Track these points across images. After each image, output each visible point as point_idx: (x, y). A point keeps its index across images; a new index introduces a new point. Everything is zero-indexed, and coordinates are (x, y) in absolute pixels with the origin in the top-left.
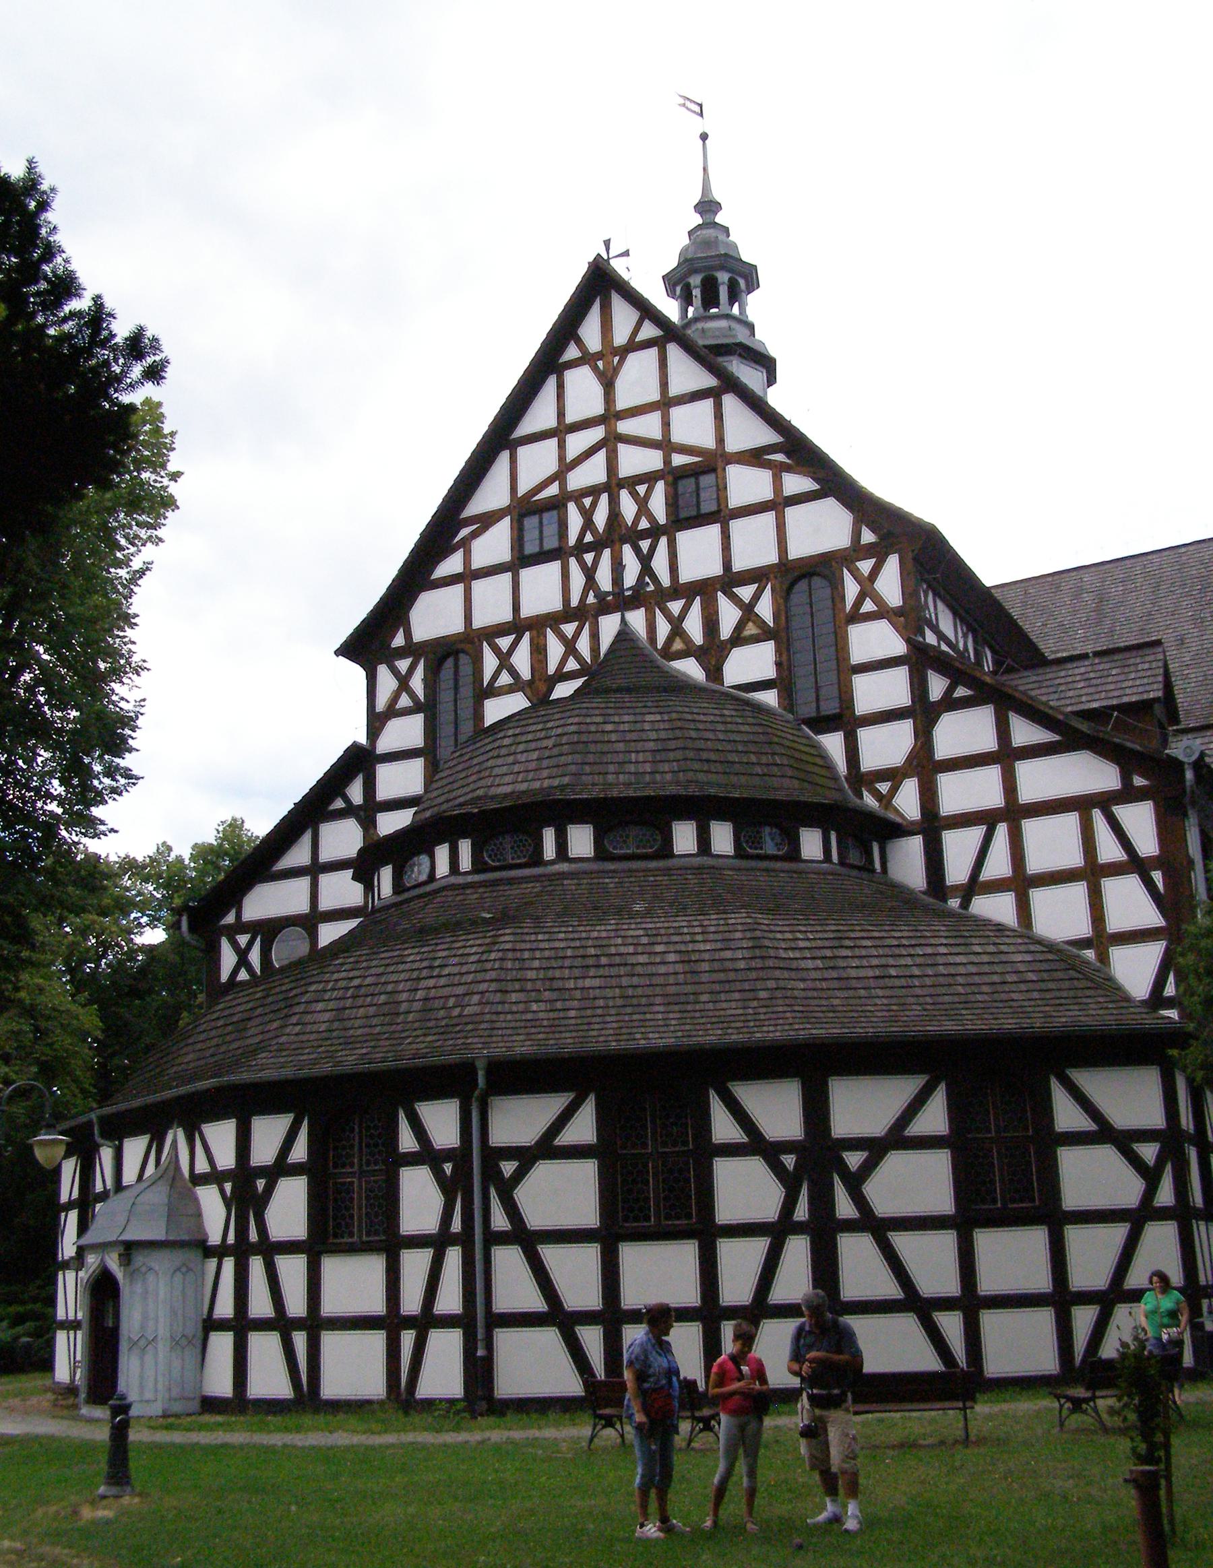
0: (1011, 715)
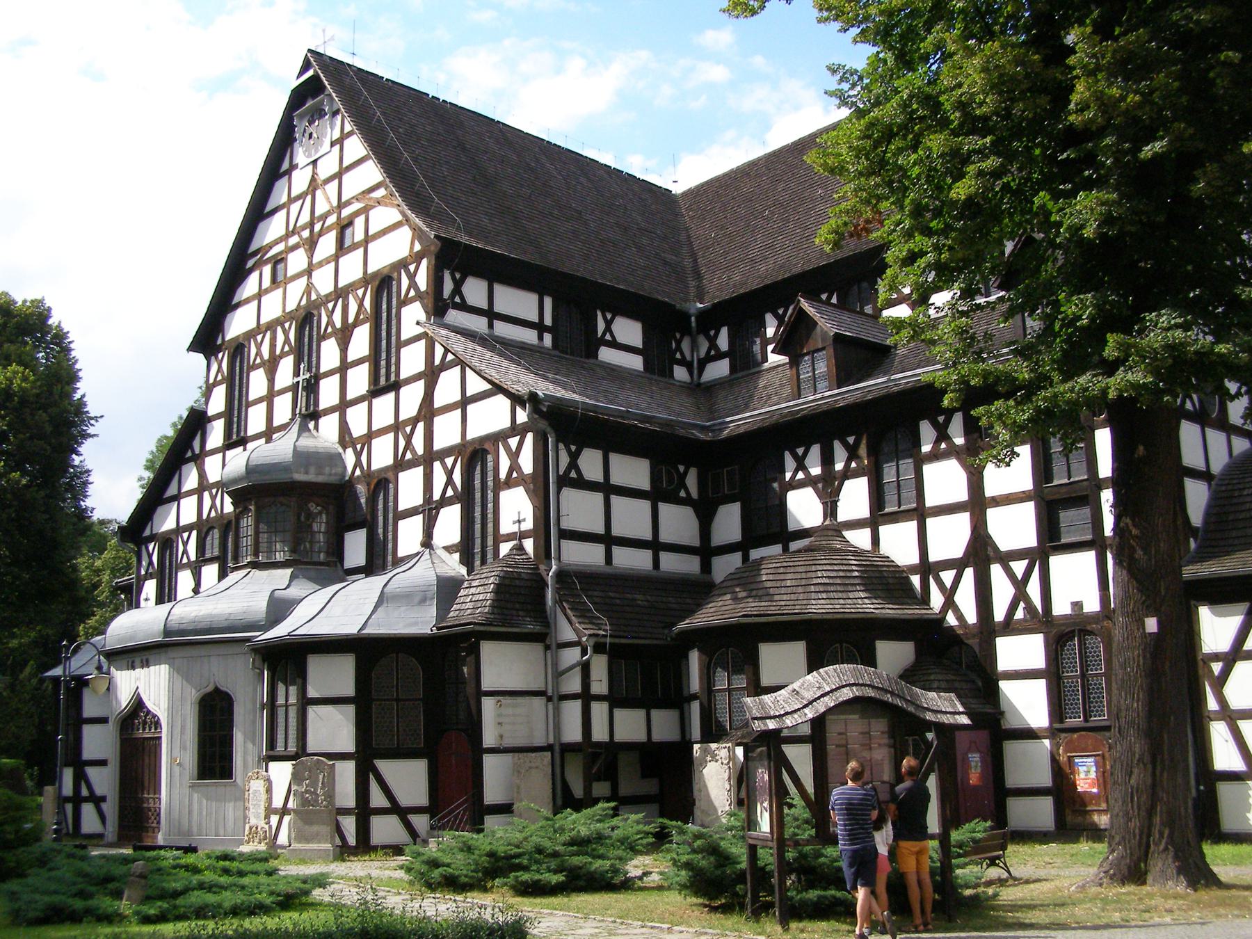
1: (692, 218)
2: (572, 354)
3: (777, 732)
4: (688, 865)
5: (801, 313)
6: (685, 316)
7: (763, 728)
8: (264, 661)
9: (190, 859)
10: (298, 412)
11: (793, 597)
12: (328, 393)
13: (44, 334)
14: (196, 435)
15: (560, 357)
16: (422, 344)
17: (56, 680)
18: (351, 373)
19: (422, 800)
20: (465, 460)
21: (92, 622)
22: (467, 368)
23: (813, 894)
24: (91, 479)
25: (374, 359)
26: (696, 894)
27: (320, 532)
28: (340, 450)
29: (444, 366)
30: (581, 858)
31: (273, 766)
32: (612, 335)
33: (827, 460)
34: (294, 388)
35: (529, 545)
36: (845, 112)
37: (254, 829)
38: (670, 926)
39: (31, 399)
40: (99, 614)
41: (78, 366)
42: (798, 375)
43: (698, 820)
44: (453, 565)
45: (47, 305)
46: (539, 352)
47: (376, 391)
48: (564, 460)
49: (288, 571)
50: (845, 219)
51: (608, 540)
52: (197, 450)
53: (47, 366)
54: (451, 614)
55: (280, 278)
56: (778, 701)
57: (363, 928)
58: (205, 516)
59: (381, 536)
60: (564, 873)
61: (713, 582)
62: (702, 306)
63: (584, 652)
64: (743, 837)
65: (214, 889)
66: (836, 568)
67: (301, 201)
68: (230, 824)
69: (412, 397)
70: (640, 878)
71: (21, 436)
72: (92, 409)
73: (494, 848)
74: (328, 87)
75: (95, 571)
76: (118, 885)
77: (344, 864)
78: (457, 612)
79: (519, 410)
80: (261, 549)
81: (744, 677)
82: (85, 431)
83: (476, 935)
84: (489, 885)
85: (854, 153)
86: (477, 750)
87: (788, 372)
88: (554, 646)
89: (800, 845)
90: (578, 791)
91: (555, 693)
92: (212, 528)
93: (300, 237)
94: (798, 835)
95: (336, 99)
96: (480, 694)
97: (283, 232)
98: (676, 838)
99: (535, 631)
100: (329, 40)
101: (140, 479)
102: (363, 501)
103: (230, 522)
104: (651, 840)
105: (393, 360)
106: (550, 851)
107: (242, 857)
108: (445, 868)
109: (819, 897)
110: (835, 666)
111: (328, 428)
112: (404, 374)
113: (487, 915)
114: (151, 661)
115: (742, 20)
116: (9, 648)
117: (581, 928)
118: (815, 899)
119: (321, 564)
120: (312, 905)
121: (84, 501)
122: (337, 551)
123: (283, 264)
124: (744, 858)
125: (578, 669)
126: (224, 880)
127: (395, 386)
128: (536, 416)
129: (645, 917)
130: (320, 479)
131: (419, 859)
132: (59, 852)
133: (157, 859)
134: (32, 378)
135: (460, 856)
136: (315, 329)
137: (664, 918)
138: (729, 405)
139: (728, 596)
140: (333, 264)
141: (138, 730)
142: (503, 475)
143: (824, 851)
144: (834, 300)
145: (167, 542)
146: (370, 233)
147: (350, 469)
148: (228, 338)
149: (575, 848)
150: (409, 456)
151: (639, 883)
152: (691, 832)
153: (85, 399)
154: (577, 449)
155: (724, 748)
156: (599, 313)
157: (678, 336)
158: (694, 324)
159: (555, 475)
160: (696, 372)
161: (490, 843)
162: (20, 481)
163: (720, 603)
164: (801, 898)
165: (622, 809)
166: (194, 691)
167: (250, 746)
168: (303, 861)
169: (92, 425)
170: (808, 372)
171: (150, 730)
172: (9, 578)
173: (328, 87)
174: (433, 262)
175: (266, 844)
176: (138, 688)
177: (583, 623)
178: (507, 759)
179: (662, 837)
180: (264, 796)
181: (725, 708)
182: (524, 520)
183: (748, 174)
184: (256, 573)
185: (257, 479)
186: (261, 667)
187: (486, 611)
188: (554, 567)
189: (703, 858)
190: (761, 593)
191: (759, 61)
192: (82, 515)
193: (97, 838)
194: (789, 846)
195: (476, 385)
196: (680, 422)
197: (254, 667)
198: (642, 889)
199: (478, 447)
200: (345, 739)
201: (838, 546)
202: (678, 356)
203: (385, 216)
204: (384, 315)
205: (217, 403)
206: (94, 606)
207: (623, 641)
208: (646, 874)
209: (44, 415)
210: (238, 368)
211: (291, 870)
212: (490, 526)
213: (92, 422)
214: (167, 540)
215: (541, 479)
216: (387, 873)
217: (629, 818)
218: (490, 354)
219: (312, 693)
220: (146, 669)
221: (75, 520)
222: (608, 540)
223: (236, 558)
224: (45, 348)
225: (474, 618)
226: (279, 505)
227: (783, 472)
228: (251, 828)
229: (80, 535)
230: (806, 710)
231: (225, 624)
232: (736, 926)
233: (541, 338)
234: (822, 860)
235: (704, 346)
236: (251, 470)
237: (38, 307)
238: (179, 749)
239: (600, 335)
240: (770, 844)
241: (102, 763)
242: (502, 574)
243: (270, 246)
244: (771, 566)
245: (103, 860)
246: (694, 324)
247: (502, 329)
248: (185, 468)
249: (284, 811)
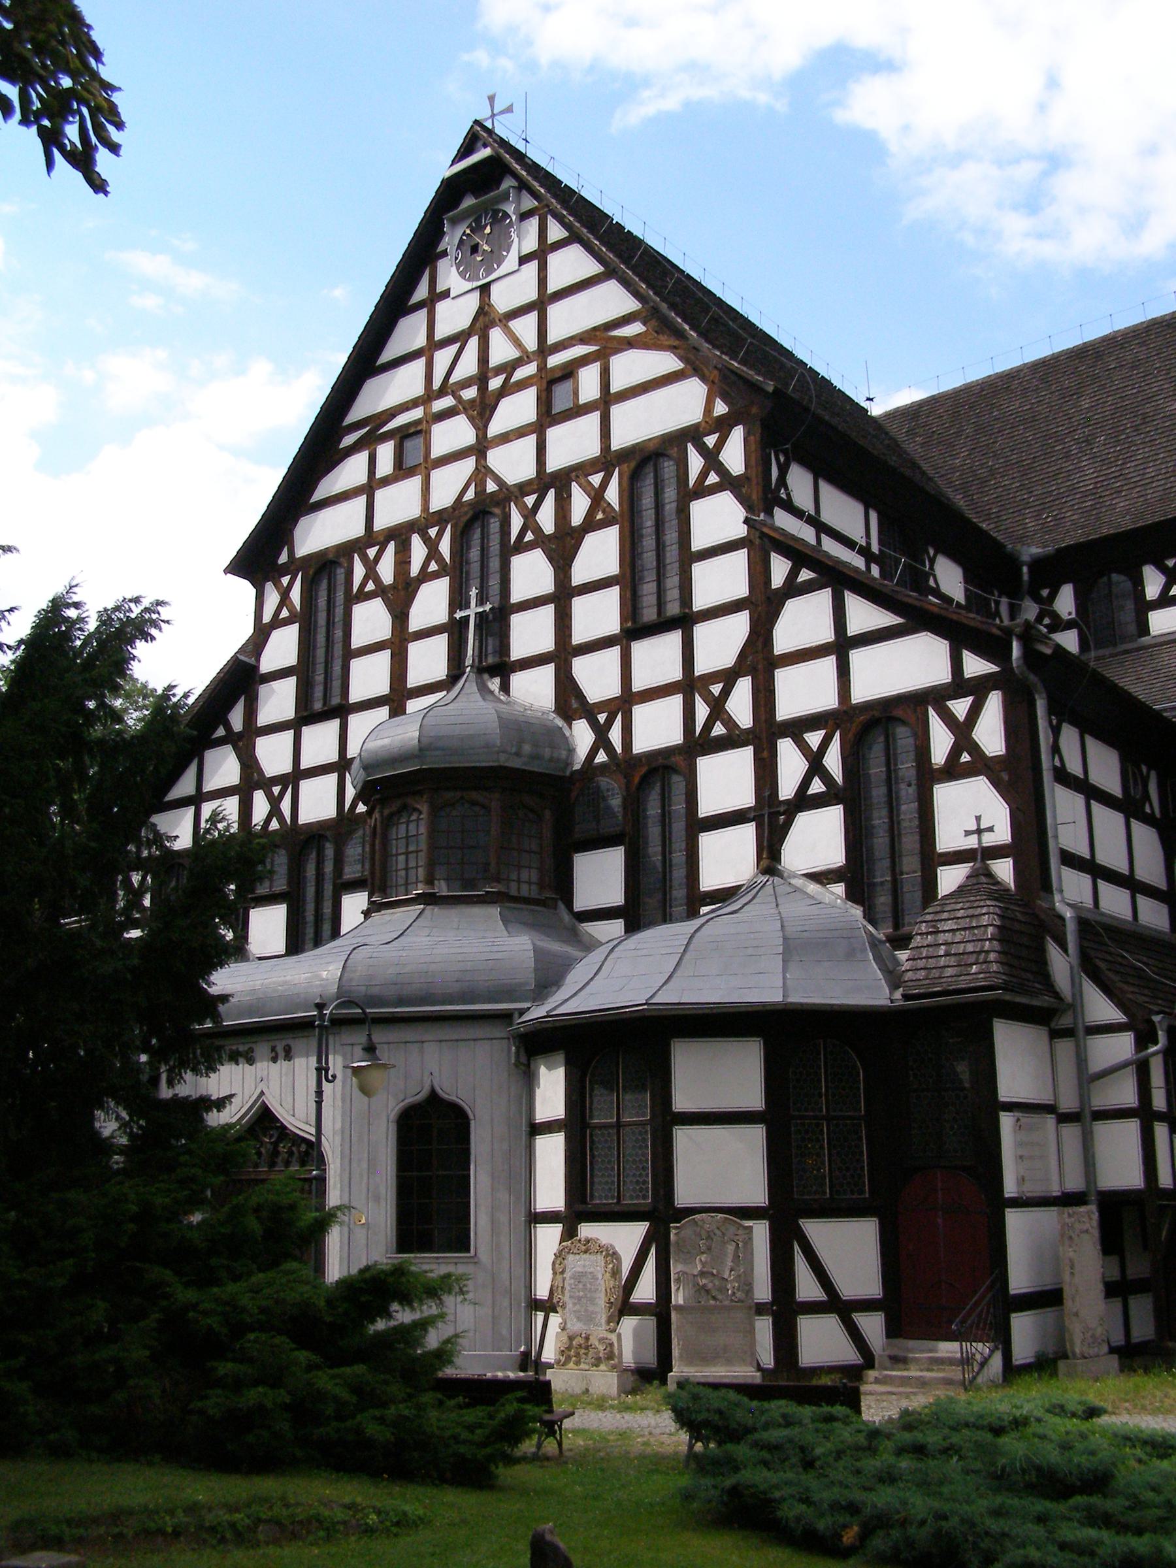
0: (847, 593)
25: (303, 671)
28: (560, 722)
35: (1004, 869)
47: (306, 716)
67: (458, 345)
86: (998, 1204)
96: (994, 1106)
97: (418, 390)
100: (502, 112)
125: (1130, 1071)
178: (1048, 1217)
220: (283, 1064)
243: (392, 413)
248: (211, 756)
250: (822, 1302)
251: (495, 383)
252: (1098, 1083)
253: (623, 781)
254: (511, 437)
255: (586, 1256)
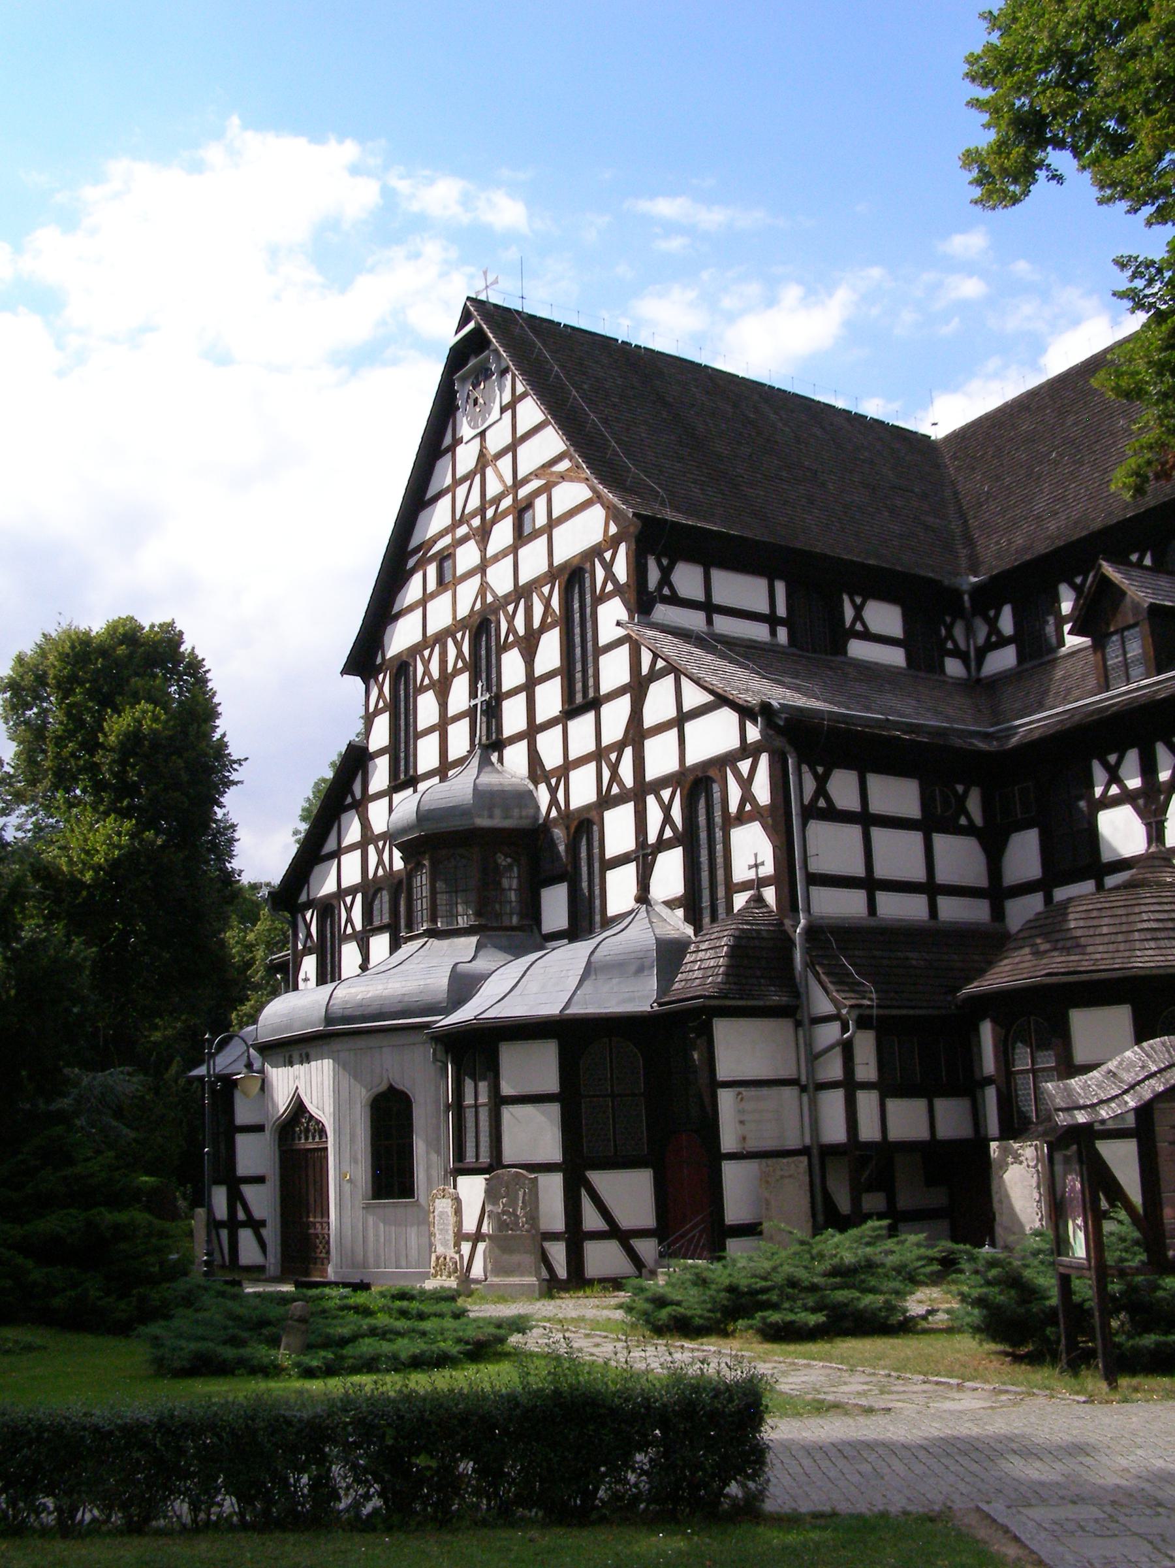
1: (958, 469)
2: (815, 651)
3: (1088, 1127)
4: (980, 1302)
5: (1105, 581)
6: (957, 594)
7: (1071, 1122)
8: (447, 1052)
9: (360, 1298)
10: (477, 742)
11: (1111, 947)
12: (513, 717)
13: (177, 663)
14: (357, 774)
15: (799, 656)
16: (624, 650)
17: (200, 1079)
18: (540, 690)
19: (648, 1220)
20: (685, 792)
21: (246, 1008)
22: (683, 677)
23: (1149, 1340)
24: (236, 835)
25: (567, 671)
26: (994, 1338)
27: (510, 889)
28: (532, 787)
29: (654, 676)
30: (845, 1292)
31: (462, 1181)
32: (864, 624)
33: (1149, 769)
34: (471, 713)
35: (769, 894)
36: (1142, 317)
37: (442, 1259)
38: (960, 1381)
39: (163, 742)
40: (254, 996)
41: (216, 700)
42: (1104, 660)
43: (1000, 1241)
44: (676, 924)
45: (178, 629)
46: (770, 651)
47: (571, 711)
48: (810, 785)
49: (474, 940)
50: (1149, 455)
51: (870, 884)
52: (358, 795)
53: (180, 703)
54: (676, 986)
55: (448, 578)
56: (1089, 1086)
57: (556, 1388)
58: (371, 875)
59: (586, 891)
60: (824, 1313)
61: (1008, 932)
62: (976, 579)
63: (845, 1028)
64: (1053, 1264)
65: (388, 1336)
66: (1167, 907)
67: (469, 482)
68: (414, 1253)
69: (616, 716)
70: (924, 1318)
71: (155, 787)
72: (235, 750)
73: (735, 1281)
74: (494, 340)
75: (247, 946)
76: (275, 1330)
77: (552, 1302)
78: (683, 983)
79: (749, 724)
80: (440, 913)
81: (1052, 1053)
82: (227, 777)
83: (697, 1398)
84: (730, 1328)
85: (1154, 369)
86: (715, 1157)
87: (1091, 658)
88: (806, 1021)
89: (1128, 1274)
90: (844, 1205)
91: (810, 1081)
92: (379, 890)
93: (470, 526)
94: (1126, 1260)
95: (504, 355)
96: (715, 1085)
97: (448, 521)
98: (965, 1266)
99: (783, 1003)
100: (492, 284)
101: (296, 833)
102: (562, 848)
103: (400, 882)
104: (936, 1267)
105: (591, 671)
106: (806, 1283)
107: (424, 1296)
108: (674, 1307)
109: (1158, 1344)
110: (1162, 1039)
111: (516, 758)
112: (605, 689)
113: (710, 1370)
114: (312, 1055)
115: (1000, 212)
116: (151, 1042)
117: (845, 1383)
118: (1153, 1346)
119: (513, 929)
120: (506, 1355)
121: (230, 862)
122: (533, 912)
123: (450, 561)
124: (1055, 1292)
125: (838, 1051)
126: (401, 1324)
127: (594, 704)
128: (771, 732)
129: (928, 1368)
130: (507, 823)
131: (643, 1296)
132: (206, 1289)
133: (321, 1298)
134: (163, 717)
135: (693, 1291)
136: (493, 638)
137: (953, 1371)
138: (1018, 705)
139: (1027, 950)
140: (511, 557)
141: (300, 1139)
142: (733, 808)
143: (1160, 1282)
144: (1148, 561)
145: (328, 909)
146: (555, 516)
147: (544, 809)
148: (389, 655)
149: (838, 1280)
150: (615, 790)
151: (924, 1324)
152: (984, 1258)
153: (225, 740)
154: (825, 771)
155: (1030, 1146)
156: (846, 598)
157: (948, 619)
158: (967, 604)
159: (799, 803)
160: (973, 664)
161: (730, 1275)
162: (155, 841)
163: (1017, 960)
164: (1132, 1346)
165: (901, 1226)
166: (363, 1091)
167: (434, 1157)
168: (502, 1299)
169: (235, 770)
170: (1117, 657)
171: (314, 1138)
172: (147, 959)
173: (494, 340)
174: (633, 547)
175: (457, 1278)
176: (297, 1088)
177: (843, 991)
179: (948, 1266)
180: (452, 1219)
181: (1029, 1094)
182: (763, 864)
183: (1028, 408)
184: (434, 943)
185: (431, 827)
186: (444, 1059)
187: (719, 980)
188: (803, 921)
189: (1001, 1293)
190: (1069, 944)
191: (1022, 267)
192: (228, 878)
193: (256, 1272)
194: (1113, 1276)
195: (694, 697)
196: (957, 730)
197: (435, 1060)
198: (925, 1331)
199: (700, 775)
200: (550, 1148)
201: (1169, 880)
202: (950, 645)
203: (569, 494)
204: (577, 616)
205: (380, 736)
206: (249, 989)
207: (895, 1012)
208: (931, 1312)
209: (179, 761)
210: (402, 692)
211: (482, 1310)
212: (720, 873)
213: (235, 766)
214: (328, 905)
215: (781, 811)
216: (607, 1313)
217: (906, 1240)
218: (710, 657)
219: (507, 1089)
221: (219, 885)
222: (870, 884)
223: (410, 926)
224: (178, 681)
225: (704, 990)
226: (458, 858)
227: (1091, 786)
228: (438, 1258)
229: (227, 903)
230: (1126, 1098)
231: (399, 1007)
232: (1047, 1382)
233: (773, 633)
234: (1160, 1293)
235: (982, 631)
236: (423, 816)
237: (169, 632)
238: (348, 1163)
239: (848, 624)
240: (1087, 1273)
241: (260, 1180)
242: (737, 933)
244: (1081, 908)
245: (258, 1300)
246: (967, 604)
247: (724, 625)
248: (345, 817)
249: (477, 1237)
250: (605, 1231)
251: (490, 513)
252: (821, 1059)
253: (565, 831)
254: (500, 557)
255: (444, 1200)
